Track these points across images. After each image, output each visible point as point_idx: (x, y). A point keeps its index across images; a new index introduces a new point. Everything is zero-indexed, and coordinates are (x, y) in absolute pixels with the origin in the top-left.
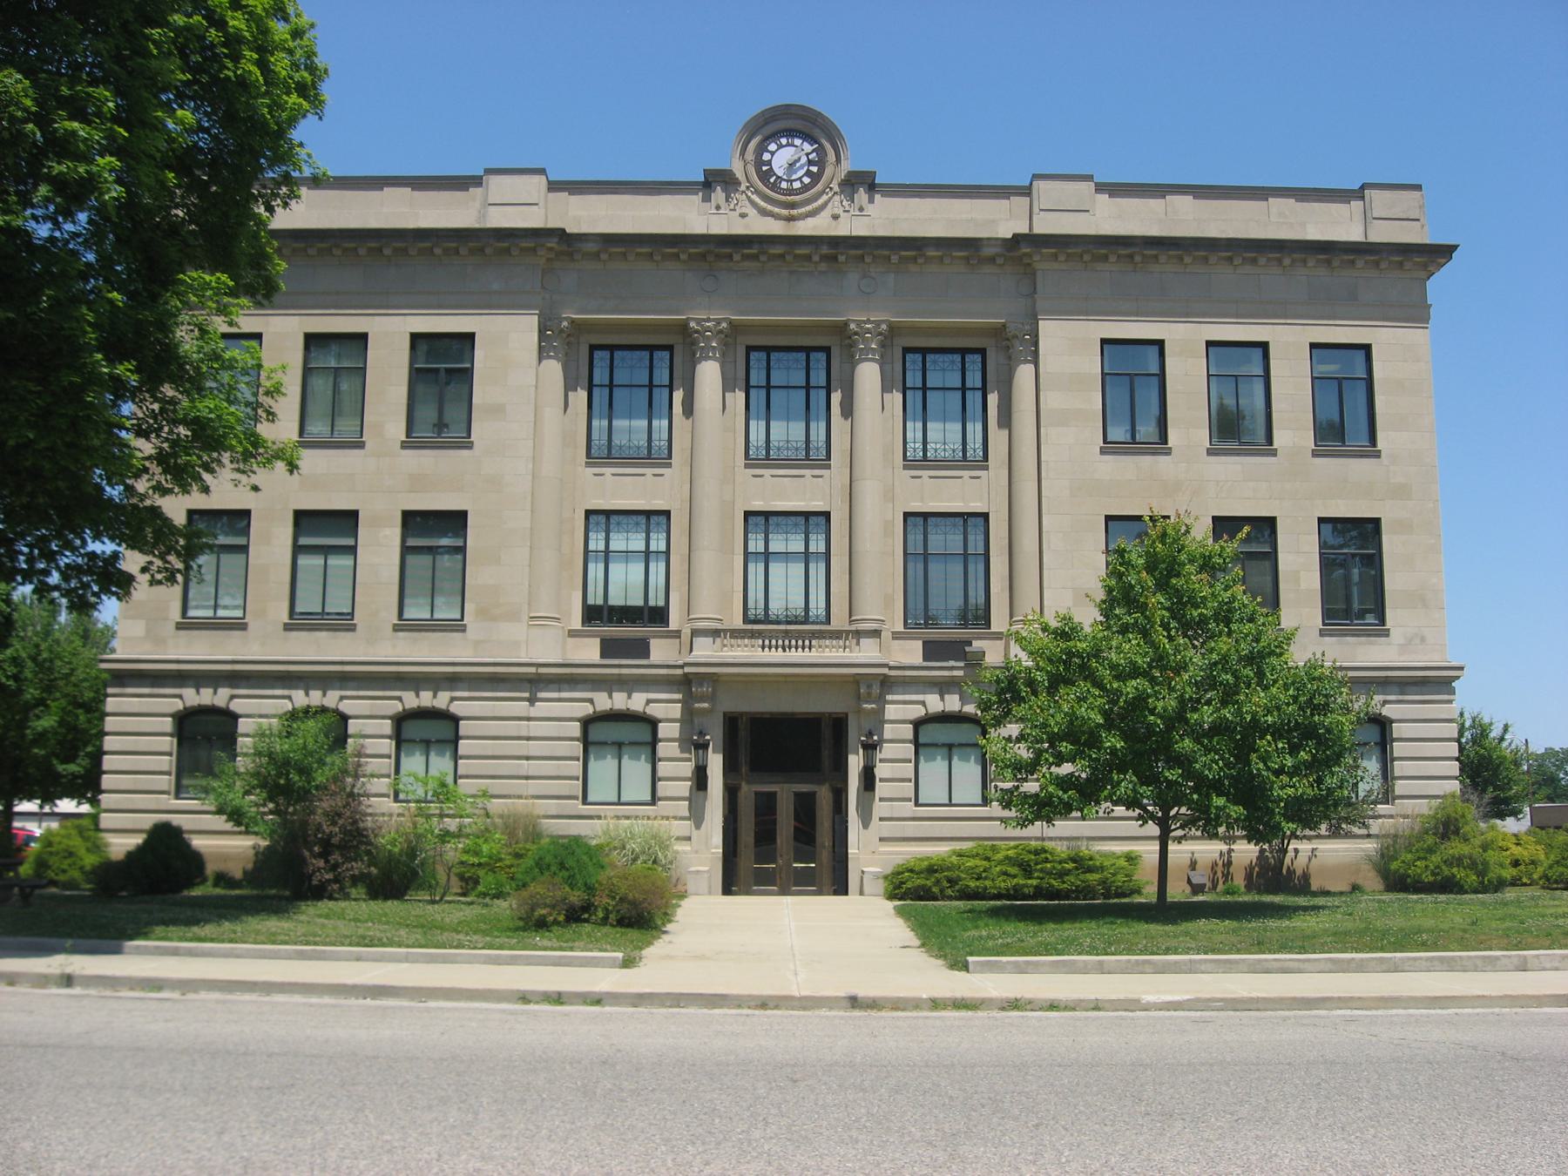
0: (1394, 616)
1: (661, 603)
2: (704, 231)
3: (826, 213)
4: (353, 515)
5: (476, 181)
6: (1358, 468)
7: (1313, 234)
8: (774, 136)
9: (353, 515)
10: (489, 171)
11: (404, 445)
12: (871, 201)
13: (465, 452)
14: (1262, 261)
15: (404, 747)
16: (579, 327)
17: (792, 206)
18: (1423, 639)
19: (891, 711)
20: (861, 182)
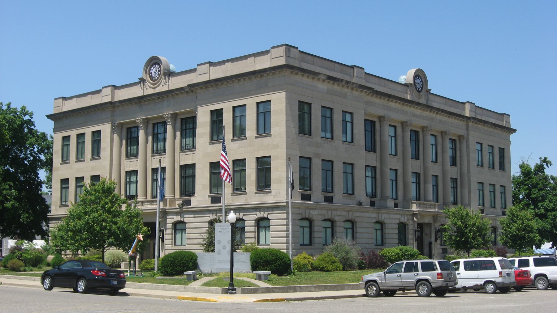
0: (273, 187)
1: (135, 194)
2: (208, 79)
3: (161, 85)
4: (83, 177)
5: (268, 52)
6: (266, 140)
7: (258, 67)
8: (152, 66)
9: (83, 177)
10: (103, 88)
11: (76, 162)
12: (169, 79)
13: (68, 165)
14: (277, 73)
15: (260, 229)
16: (122, 125)
17: (155, 84)
18: (280, 194)
19: (169, 221)
20: (170, 74)
